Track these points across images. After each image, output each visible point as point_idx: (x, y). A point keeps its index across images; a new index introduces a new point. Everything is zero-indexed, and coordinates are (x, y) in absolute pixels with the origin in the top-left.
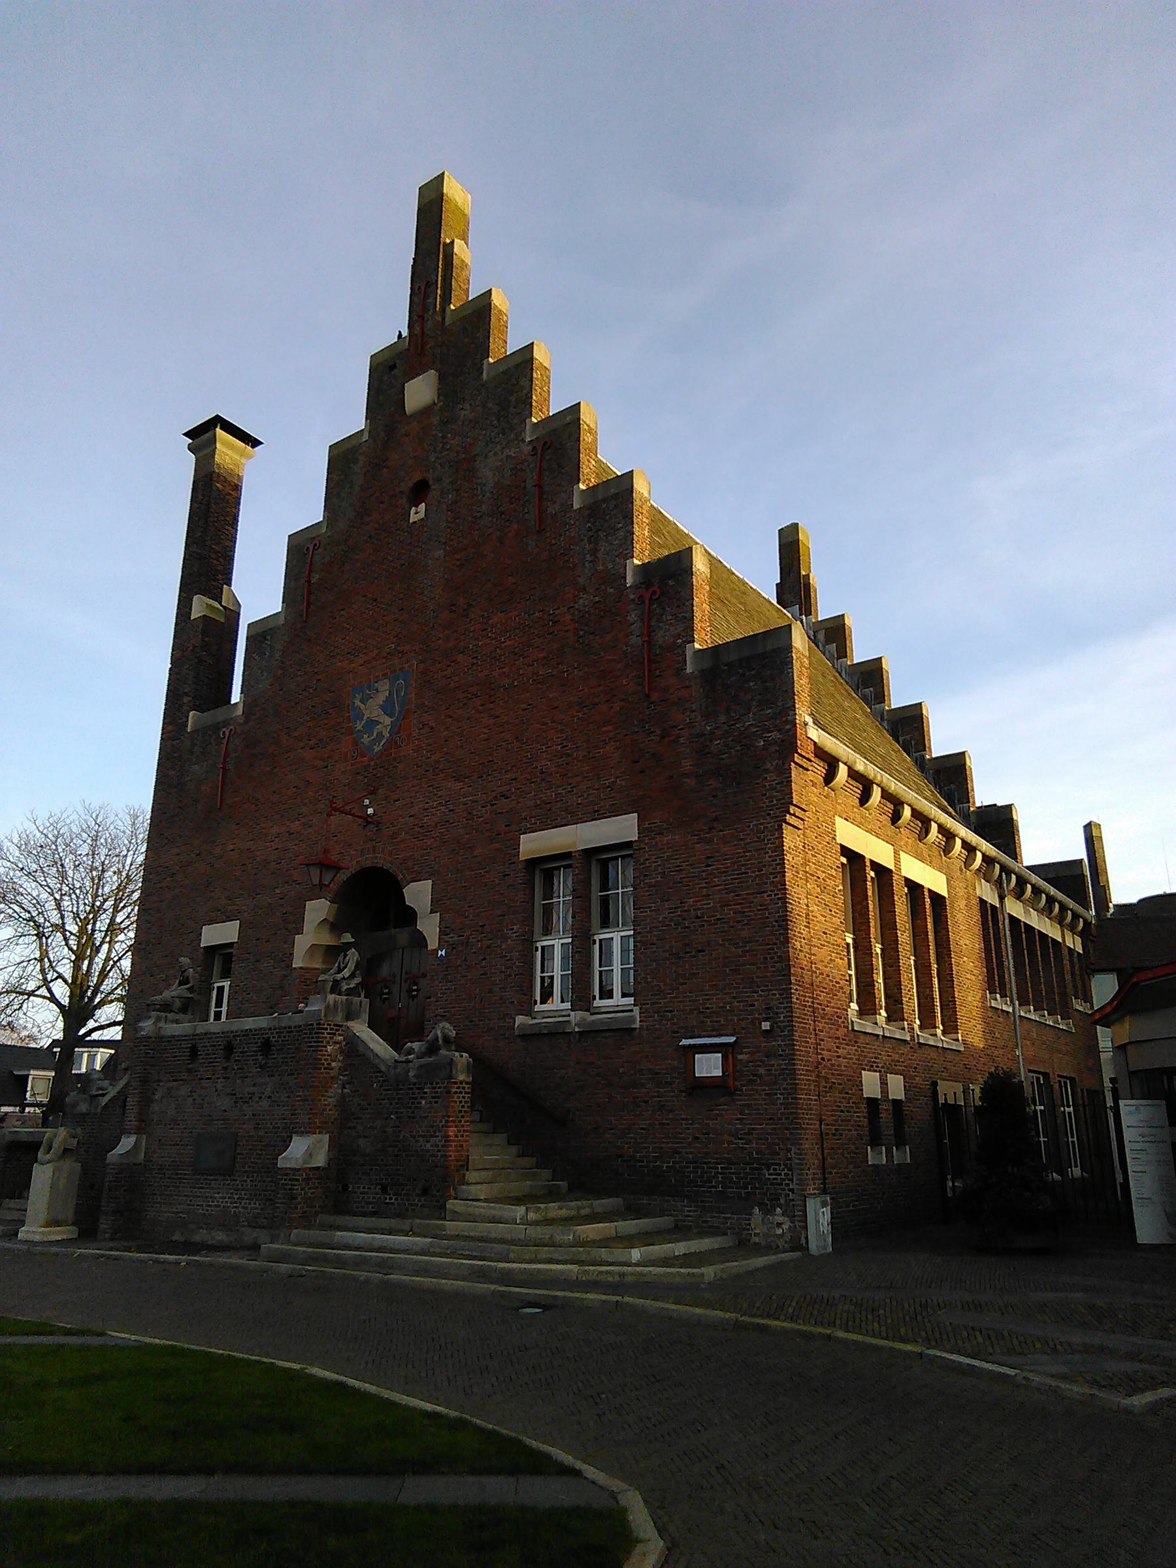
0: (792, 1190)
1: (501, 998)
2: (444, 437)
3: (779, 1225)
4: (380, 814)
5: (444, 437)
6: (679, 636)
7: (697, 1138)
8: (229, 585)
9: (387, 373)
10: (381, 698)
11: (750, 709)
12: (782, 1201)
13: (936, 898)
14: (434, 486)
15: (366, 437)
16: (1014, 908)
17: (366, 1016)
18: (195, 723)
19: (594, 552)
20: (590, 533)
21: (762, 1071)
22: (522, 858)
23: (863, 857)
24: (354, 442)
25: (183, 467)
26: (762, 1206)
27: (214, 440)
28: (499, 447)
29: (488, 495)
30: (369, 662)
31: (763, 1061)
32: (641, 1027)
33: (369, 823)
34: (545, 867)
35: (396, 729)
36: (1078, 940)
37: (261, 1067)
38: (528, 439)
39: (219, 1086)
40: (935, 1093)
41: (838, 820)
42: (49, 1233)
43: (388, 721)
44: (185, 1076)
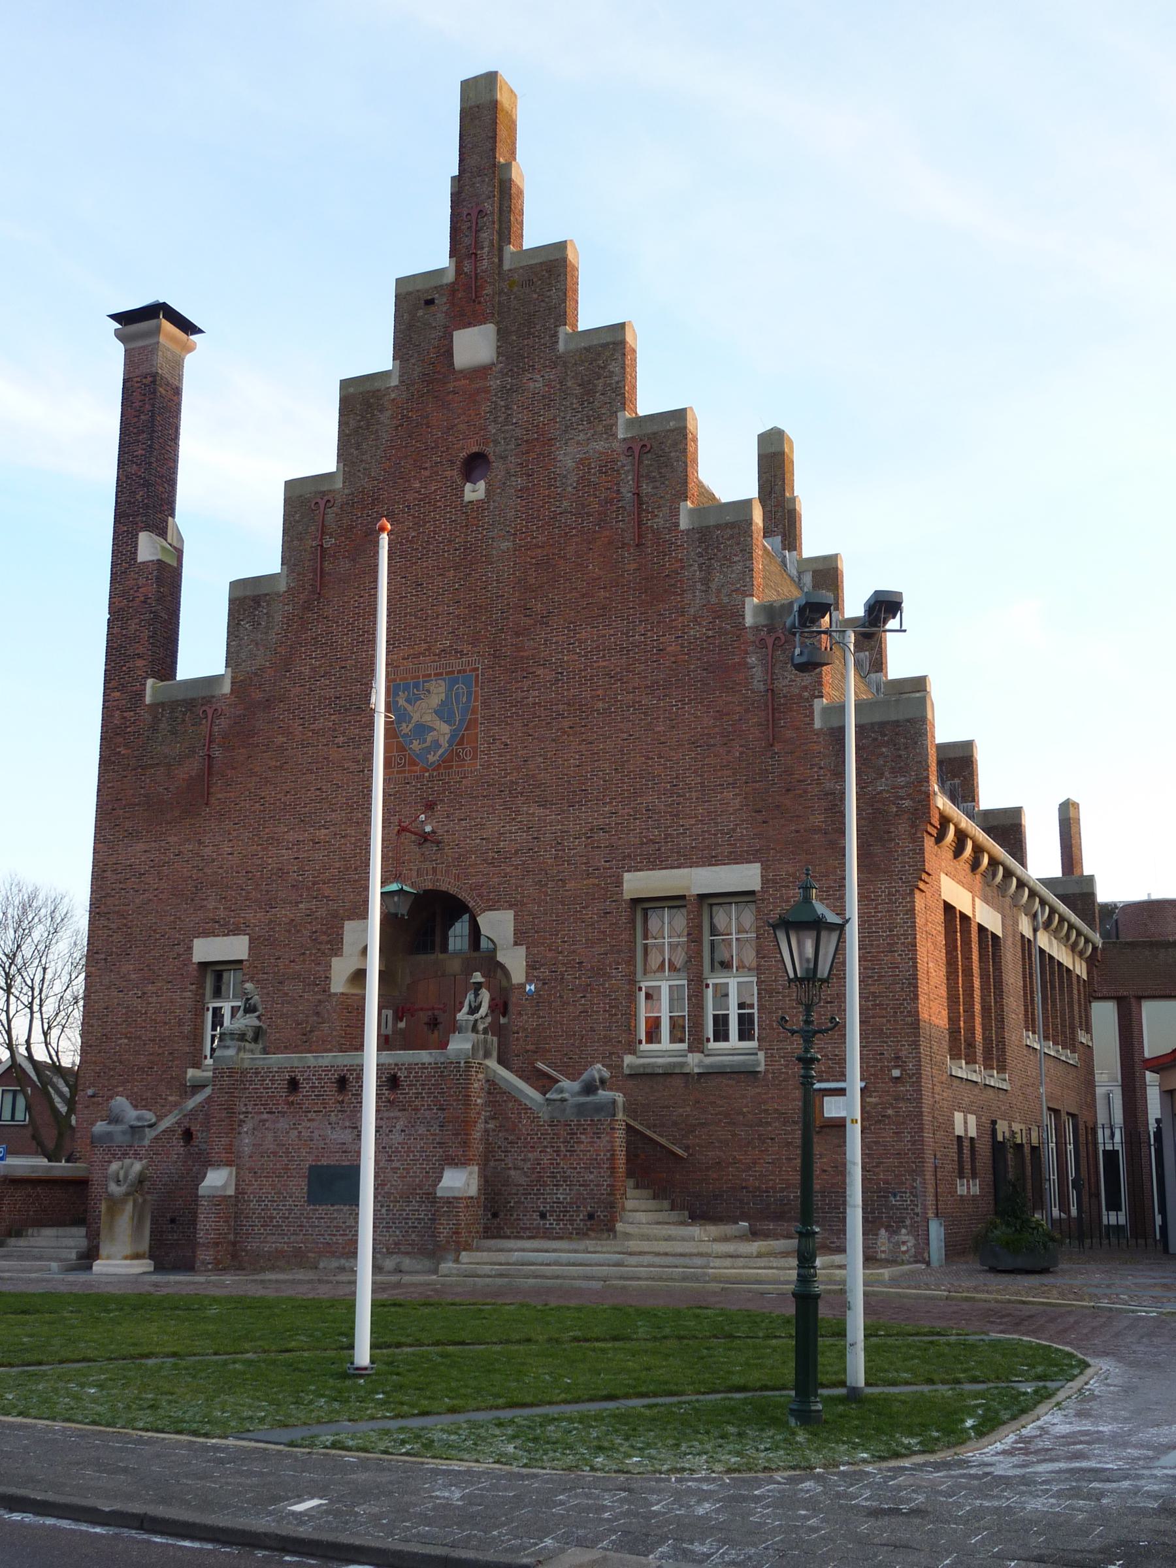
0: (917, 1215)
1: (605, 1037)
2: (507, 407)
3: (904, 1243)
4: (440, 832)
5: (507, 407)
6: (805, 688)
7: (825, 1171)
8: (173, 517)
9: (422, 310)
10: (435, 701)
11: (882, 774)
12: (908, 1222)
13: (994, 936)
14: (497, 465)
15: (394, 382)
16: (1044, 941)
17: (495, 1054)
18: (153, 695)
19: (706, 581)
20: (701, 560)
21: (890, 1112)
22: (627, 895)
23: (954, 908)
24: (377, 385)
25: (110, 361)
26: (888, 1228)
27: (158, 330)
28: (582, 437)
29: (570, 489)
30: (416, 656)
31: (891, 1104)
32: (766, 1071)
33: (426, 840)
34: (644, 905)
35: (458, 740)
36: (1084, 965)
37: (389, 1101)
38: (620, 436)
39: (333, 1119)
40: (994, 1132)
41: (943, 876)
42: (127, 1266)
43: (445, 728)
44: (283, 1107)
